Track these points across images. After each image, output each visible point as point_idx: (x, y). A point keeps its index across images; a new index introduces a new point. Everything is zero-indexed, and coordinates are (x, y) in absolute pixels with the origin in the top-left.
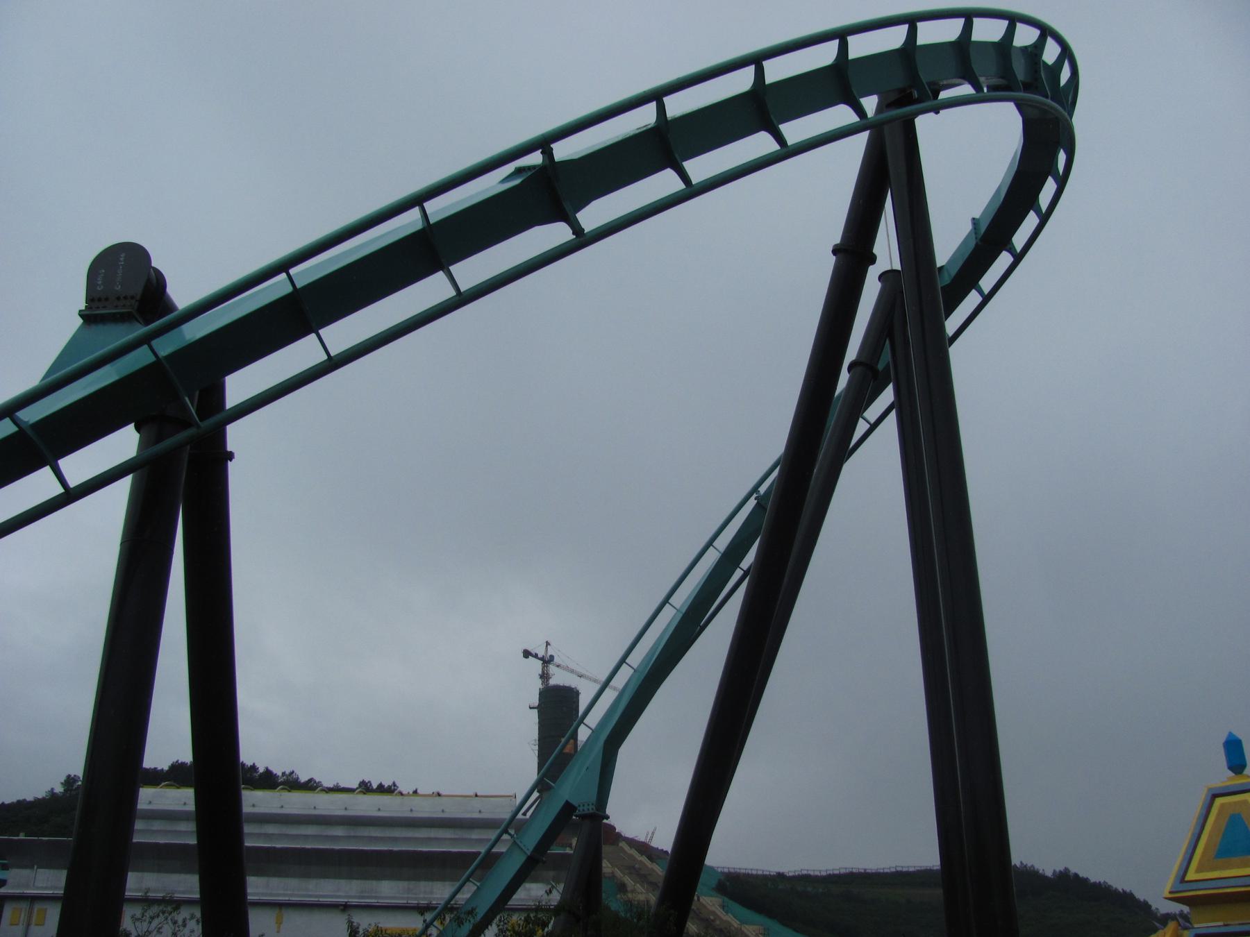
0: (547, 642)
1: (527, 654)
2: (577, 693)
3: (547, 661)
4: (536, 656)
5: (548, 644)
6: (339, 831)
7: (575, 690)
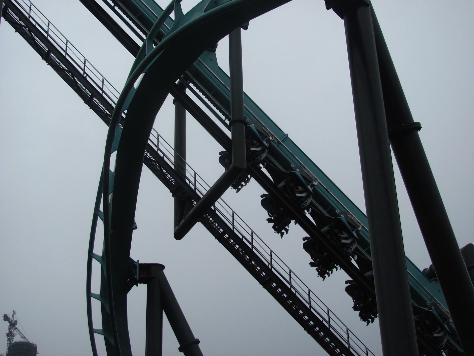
0: (14, 311)
7: (34, 346)
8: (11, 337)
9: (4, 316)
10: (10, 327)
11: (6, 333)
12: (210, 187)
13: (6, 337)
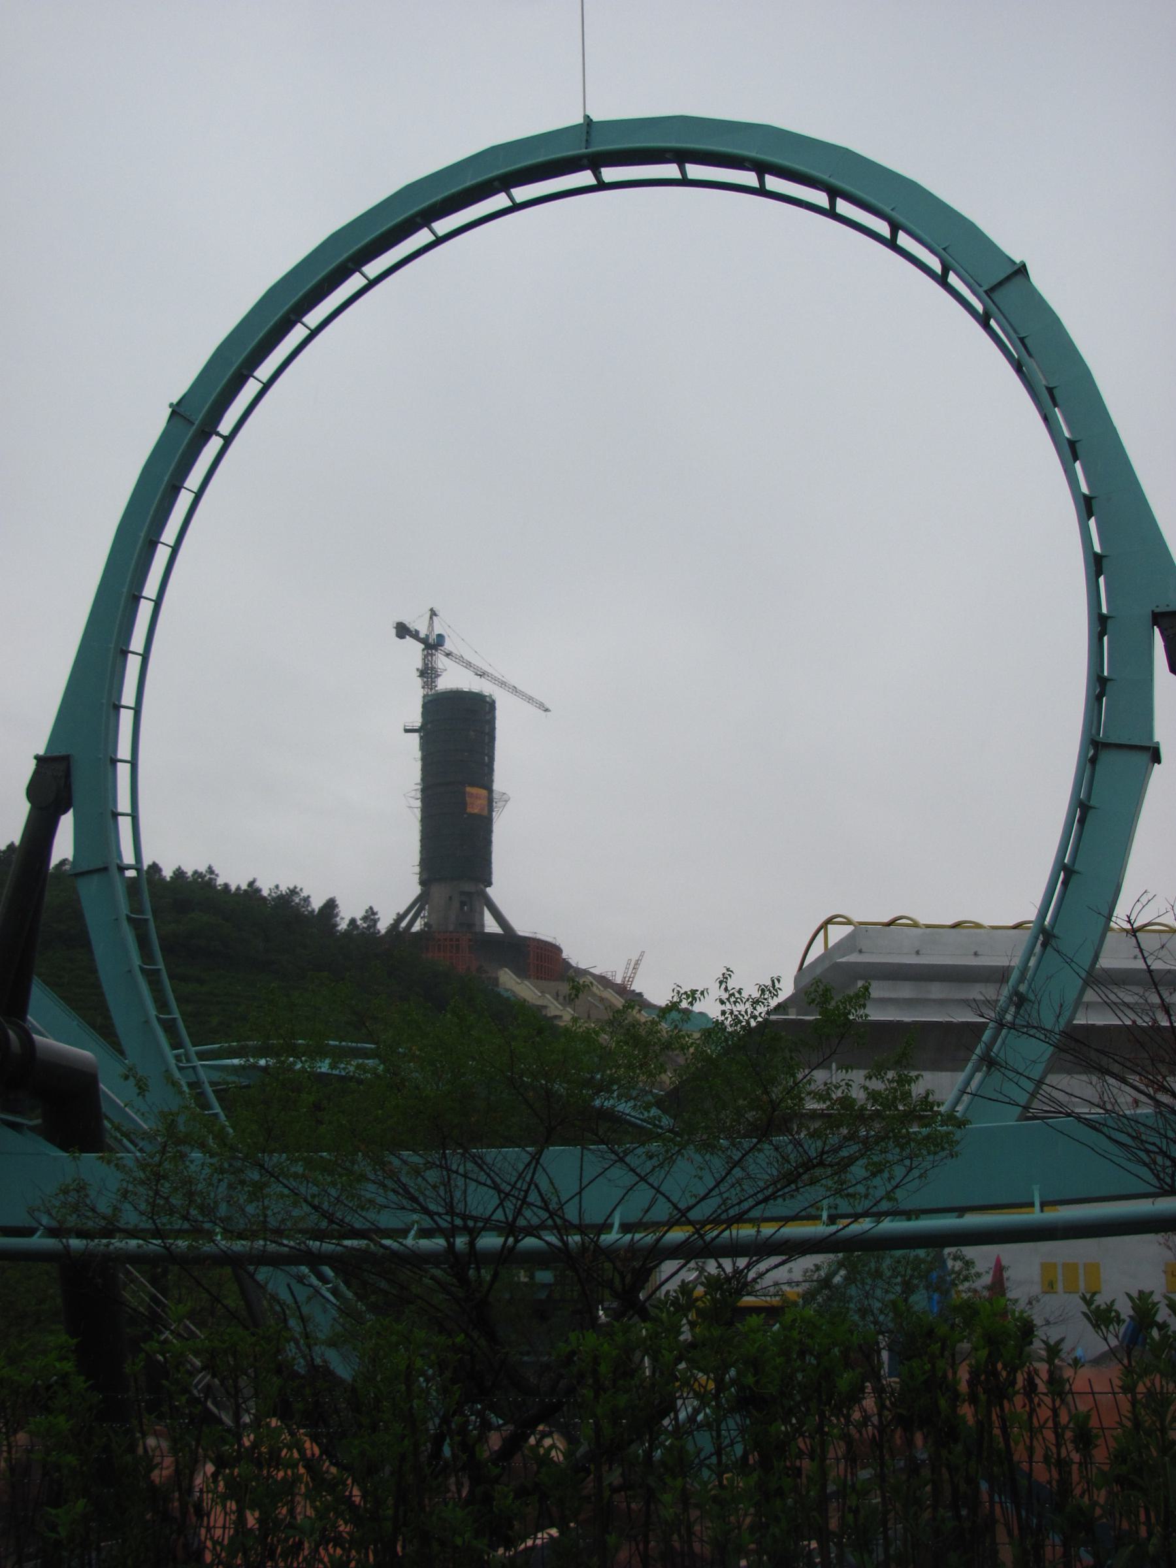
0: (432, 610)
1: (403, 631)
2: (492, 705)
3: (433, 645)
4: (415, 635)
5: (433, 613)
6: (936, 991)
7: (488, 699)
8: (432, 678)
9: (395, 625)
10: (425, 652)
11: (418, 670)
12: (1109, 1346)
13: (419, 679)
